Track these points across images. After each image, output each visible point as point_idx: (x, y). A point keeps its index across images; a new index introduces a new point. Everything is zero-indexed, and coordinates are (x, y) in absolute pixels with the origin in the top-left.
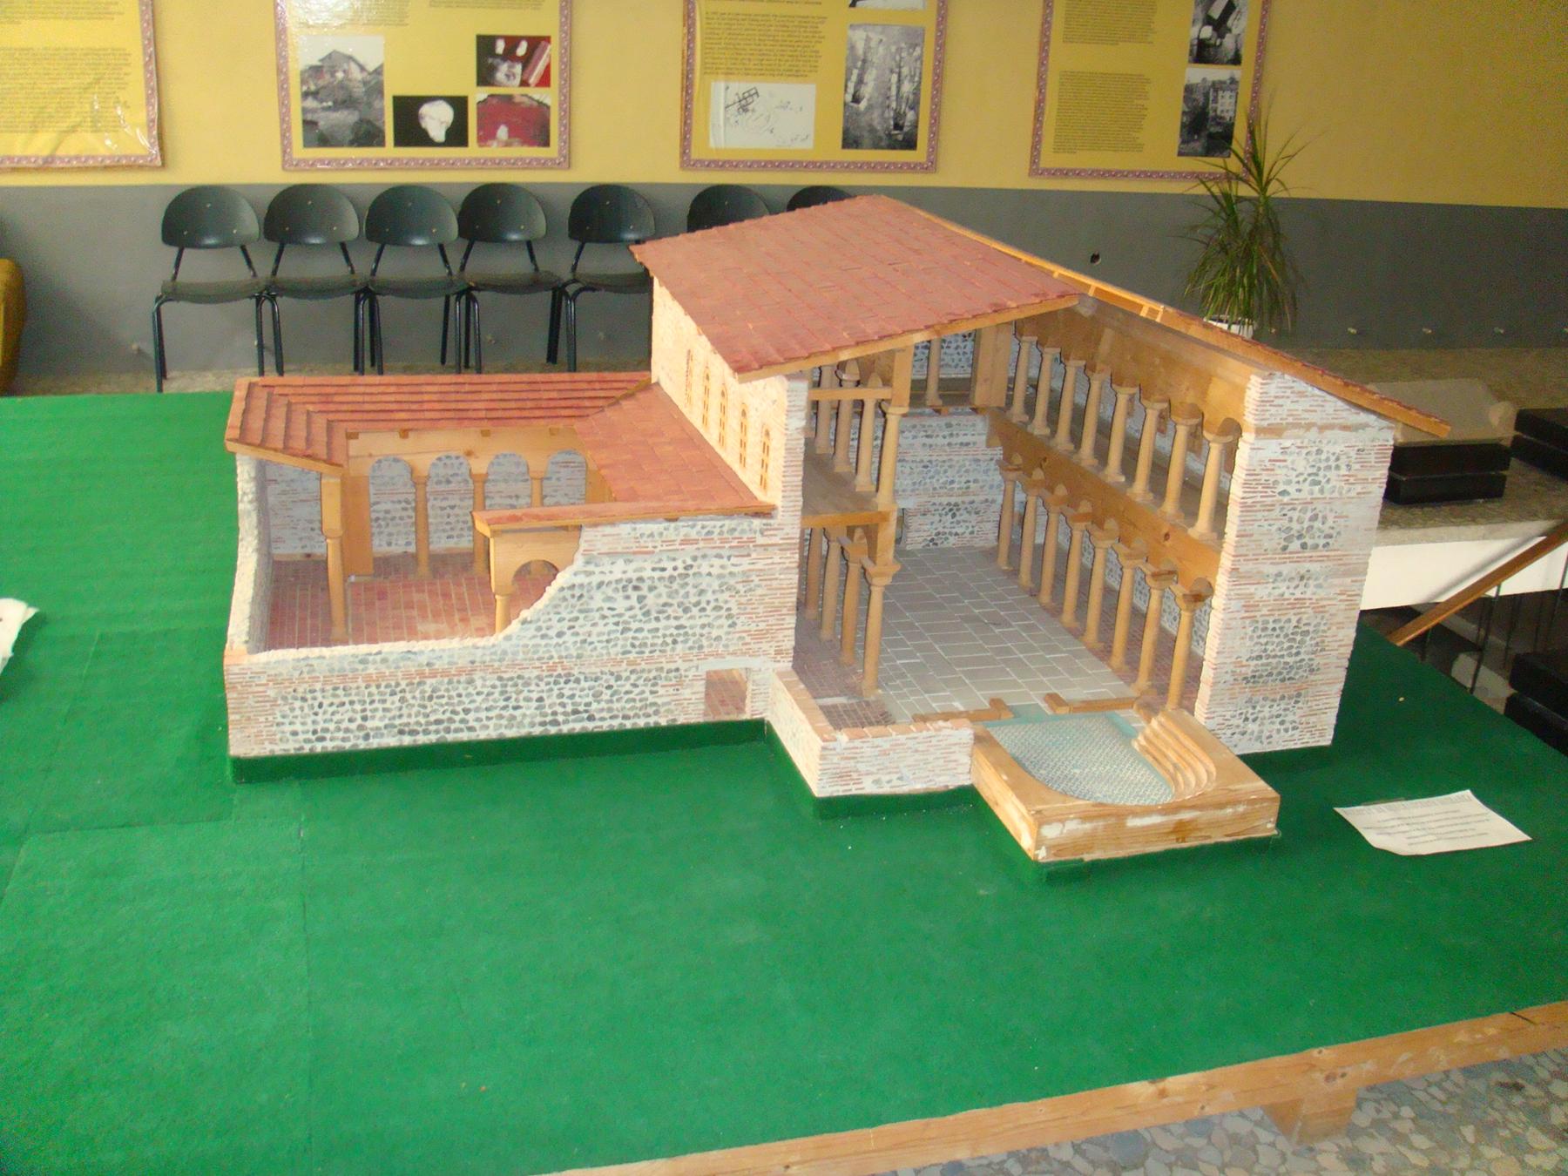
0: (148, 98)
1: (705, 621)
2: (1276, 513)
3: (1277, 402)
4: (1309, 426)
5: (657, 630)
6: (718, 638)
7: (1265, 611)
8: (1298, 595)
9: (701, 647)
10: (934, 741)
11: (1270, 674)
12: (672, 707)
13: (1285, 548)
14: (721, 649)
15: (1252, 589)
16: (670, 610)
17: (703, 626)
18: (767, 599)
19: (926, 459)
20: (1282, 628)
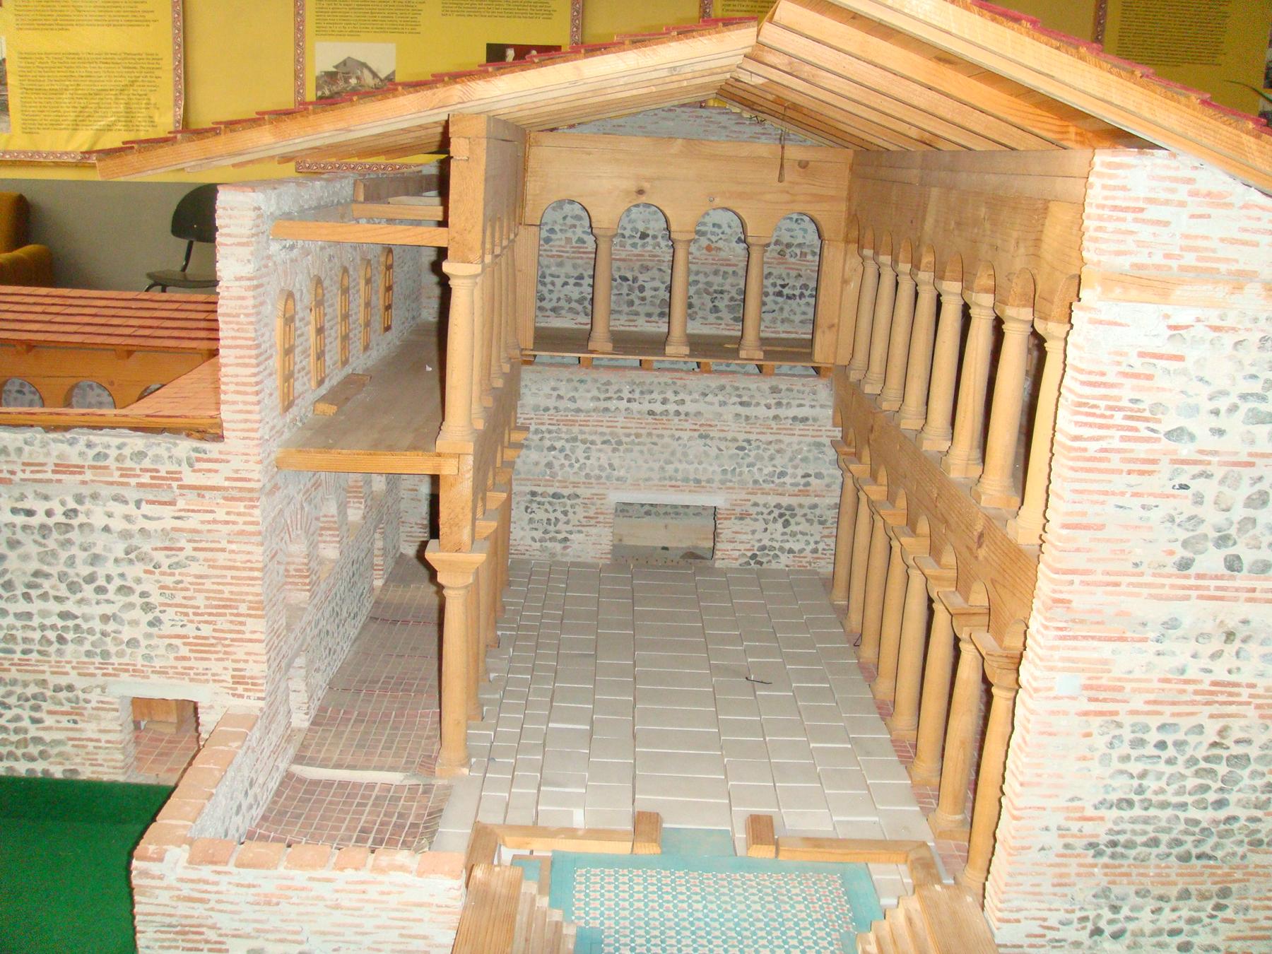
0: (176, 100)
1: (108, 609)
2: (1161, 480)
3: (1153, 212)
4: (1239, 280)
5: (29, 615)
6: (132, 643)
7: (1138, 703)
8: (1220, 674)
9: (106, 654)
10: (373, 892)
11: (1155, 842)
12: (68, 748)
13: (1185, 565)
14: (140, 662)
15: (1106, 649)
16: (46, 585)
17: (105, 618)
18: (208, 585)
19: (742, 436)
20: (1179, 744)
